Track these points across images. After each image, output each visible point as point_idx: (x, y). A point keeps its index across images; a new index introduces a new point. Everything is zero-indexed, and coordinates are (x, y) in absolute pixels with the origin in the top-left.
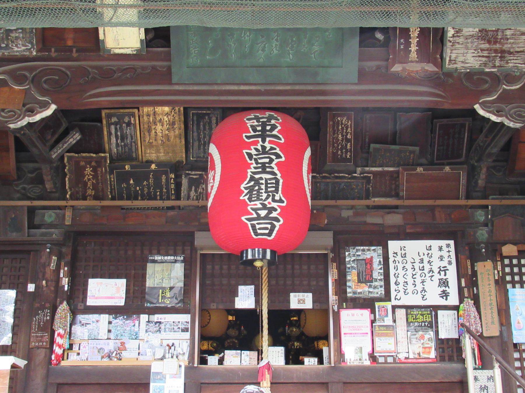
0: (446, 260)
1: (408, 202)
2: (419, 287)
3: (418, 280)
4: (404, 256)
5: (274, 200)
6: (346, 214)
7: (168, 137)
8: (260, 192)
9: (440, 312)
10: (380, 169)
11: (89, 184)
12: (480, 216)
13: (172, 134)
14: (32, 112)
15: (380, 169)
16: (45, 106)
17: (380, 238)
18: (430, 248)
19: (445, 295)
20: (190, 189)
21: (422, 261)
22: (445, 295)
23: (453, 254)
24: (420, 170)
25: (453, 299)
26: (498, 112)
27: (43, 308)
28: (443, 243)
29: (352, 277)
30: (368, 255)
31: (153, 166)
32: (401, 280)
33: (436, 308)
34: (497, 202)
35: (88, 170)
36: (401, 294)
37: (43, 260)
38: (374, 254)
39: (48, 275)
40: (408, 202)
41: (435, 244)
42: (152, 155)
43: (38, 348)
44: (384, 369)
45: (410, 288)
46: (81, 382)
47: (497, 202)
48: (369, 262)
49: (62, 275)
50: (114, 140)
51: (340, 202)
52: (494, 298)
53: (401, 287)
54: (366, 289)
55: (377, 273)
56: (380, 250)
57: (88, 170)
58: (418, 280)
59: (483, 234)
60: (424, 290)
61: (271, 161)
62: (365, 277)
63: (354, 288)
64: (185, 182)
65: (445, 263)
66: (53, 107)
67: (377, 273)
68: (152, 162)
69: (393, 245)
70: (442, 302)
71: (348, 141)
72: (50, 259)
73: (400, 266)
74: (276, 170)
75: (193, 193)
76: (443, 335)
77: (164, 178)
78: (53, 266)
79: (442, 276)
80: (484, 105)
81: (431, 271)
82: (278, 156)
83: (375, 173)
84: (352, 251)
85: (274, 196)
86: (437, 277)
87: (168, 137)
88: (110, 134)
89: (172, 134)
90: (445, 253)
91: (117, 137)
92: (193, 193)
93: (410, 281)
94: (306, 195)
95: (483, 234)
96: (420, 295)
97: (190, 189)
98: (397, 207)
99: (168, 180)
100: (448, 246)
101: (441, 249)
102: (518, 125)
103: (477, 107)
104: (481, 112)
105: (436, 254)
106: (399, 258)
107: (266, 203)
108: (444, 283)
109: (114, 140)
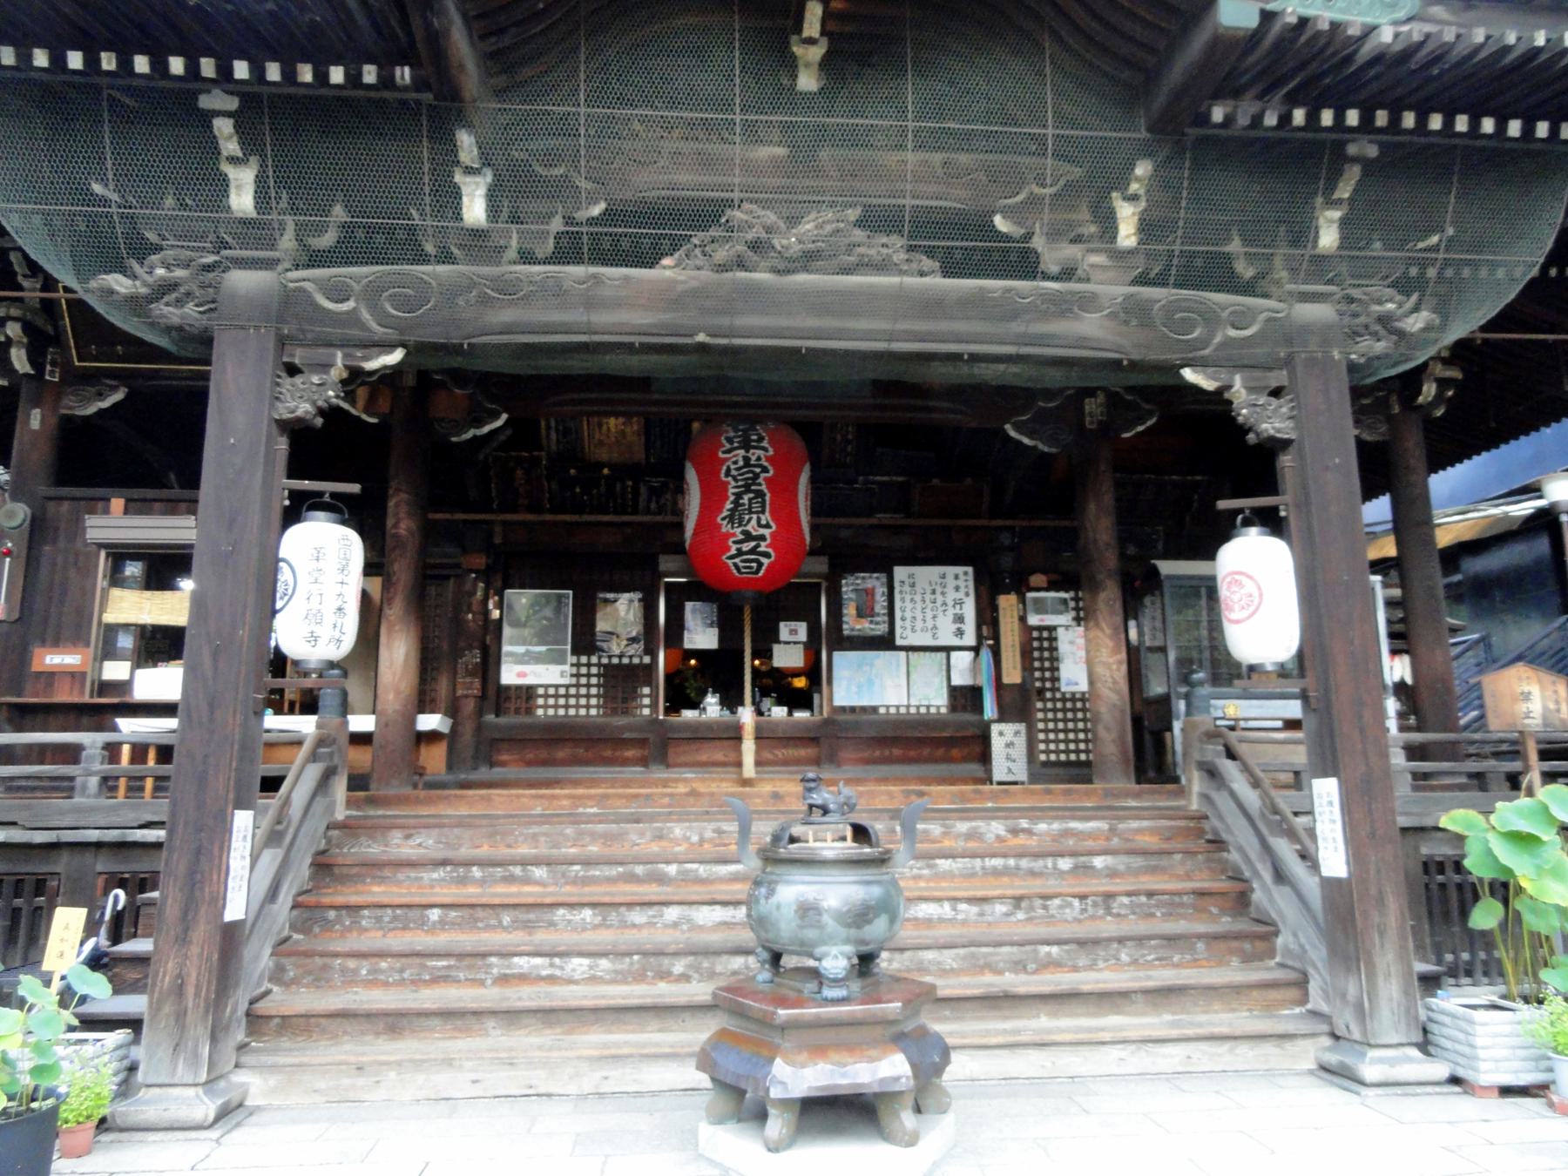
0: (963, 590)
1: (921, 522)
2: (930, 624)
3: (929, 614)
4: (913, 585)
5: (760, 525)
6: (844, 533)
7: (623, 433)
8: (745, 515)
9: (954, 655)
10: (885, 478)
11: (521, 490)
12: (1006, 539)
13: (628, 430)
14: (479, 423)
15: (885, 478)
16: (496, 416)
17: (884, 565)
18: (943, 576)
19: (960, 633)
20: (649, 501)
21: (934, 592)
22: (960, 633)
23: (971, 584)
24: (935, 481)
25: (970, 639)
26: (1031, 436)
27: (470, 648)
28: (960, 570)
29: (850, 611)
30: (869, 584)
31: (606, 471)
32: (908, 615)
33: (948, 650)
34: (1025, 523)
35: (519, 473)
36: (908, 632)
37: (468, 586)
38: (876, 582)
39: (475, 607)
40: (921, 522)
41: (951, 570)
42: (603, 455)
43: (467, 696)
44: (886, 722)
45: (919, 624)
46: (1192, 1046)
47: (1025, 523)
48: (870, 593)
49: (491, 606)
50: (554, 436)
51: (838, 521)
52: (1017, 639)
53: (908, 624)
54: (867, 625)
55: (880, 605)
56: (883, 577)
57: (519, 473)
58: (929, 614)
59: (1007, 561)
60: (935, 627)
61: (757, 476)
62: (864, 612)
63: (852, 623)
64: (643, 490)
65: (960, 595)
66: (505, 416)
67: (880, 605)
68: (603, 465)
69: (900, 572)
70: (956, 642)
71: (848, 442)
72: (475, 586)
73: (908, 597)
74: (764, 487)
75: (653, 506)
76: (957, 680)
77: (618, 487)
78: (479, 594)
79: (957, 611)
80: (1017, 427)
81: (945, 604)
82: (765, 470)
83: (880, 484)
84: (851, 579)
85: (759, 520)
86: (951, 612)
87: (623, 433)
88: (548, 428)
89: (628, 430)
90: (961, 583)
91: (557, 431)
92: (653, 506)
93: (919, 616)
94: (799, 523)
95: (1007, 561)
96: (930, 634)
97: (649, 501)
98: (907, 527)
99: (624, 488)
100: (966, 573)
101: (957, 577)
102: (1054, 450)
103: (1007, 427)
104: (1013, 434)
105: (951, 583)
106: (907, 588)
107: (749, 528)
108: (959, 619)
109: (554, 436)
